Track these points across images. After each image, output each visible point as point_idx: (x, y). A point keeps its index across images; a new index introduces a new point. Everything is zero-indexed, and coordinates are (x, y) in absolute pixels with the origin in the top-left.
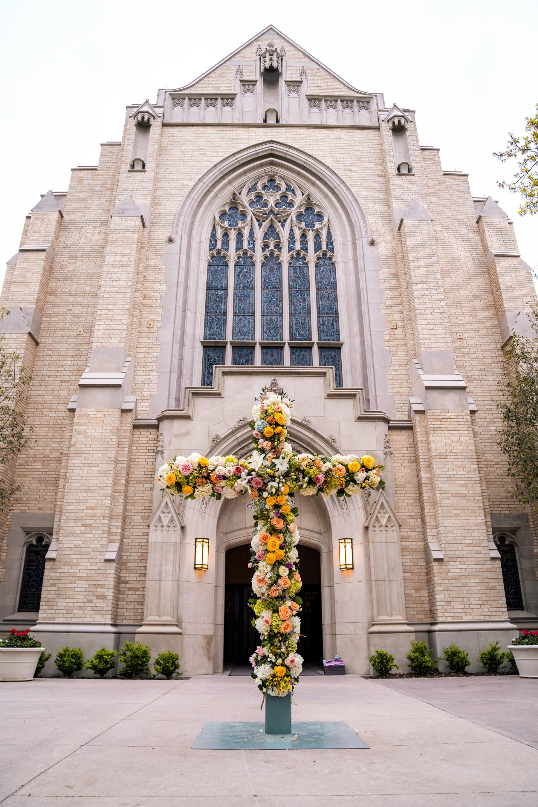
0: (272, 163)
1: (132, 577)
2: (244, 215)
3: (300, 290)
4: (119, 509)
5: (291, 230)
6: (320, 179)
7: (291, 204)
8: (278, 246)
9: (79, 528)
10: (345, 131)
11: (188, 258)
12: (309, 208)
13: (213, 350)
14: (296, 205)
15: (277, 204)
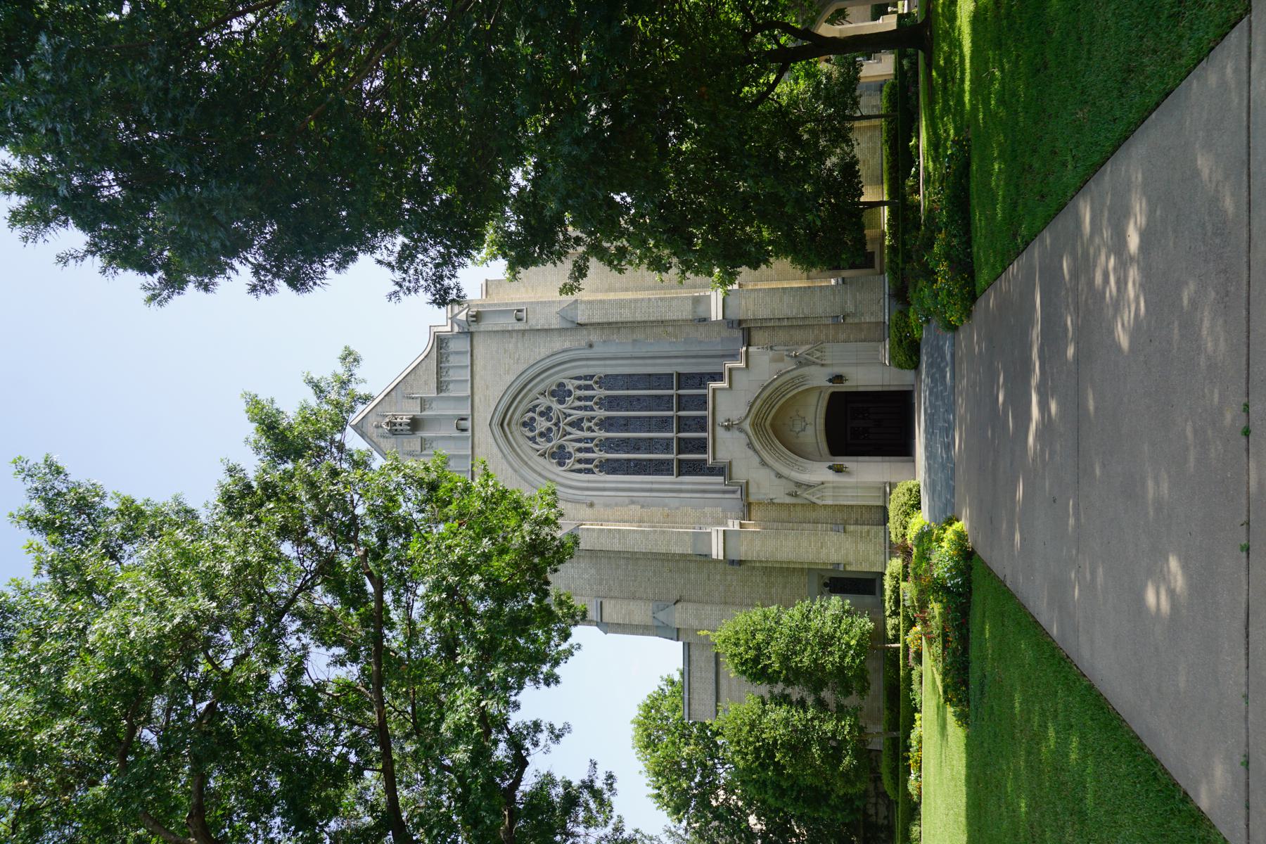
0: (509, 424)
1: (854, 516)
2: (561, 447)
3: (631, 402)
4: (810, 526)
5: (574, 408)
6: (526, 385)
7: (549, 409)
8: (590, 419)
9: (824, 551)
10: (476, 362)
11: (604, 489)
12: (553, 394)
13: (688, 468)
14: (549, 403)
15: (549, 419)
